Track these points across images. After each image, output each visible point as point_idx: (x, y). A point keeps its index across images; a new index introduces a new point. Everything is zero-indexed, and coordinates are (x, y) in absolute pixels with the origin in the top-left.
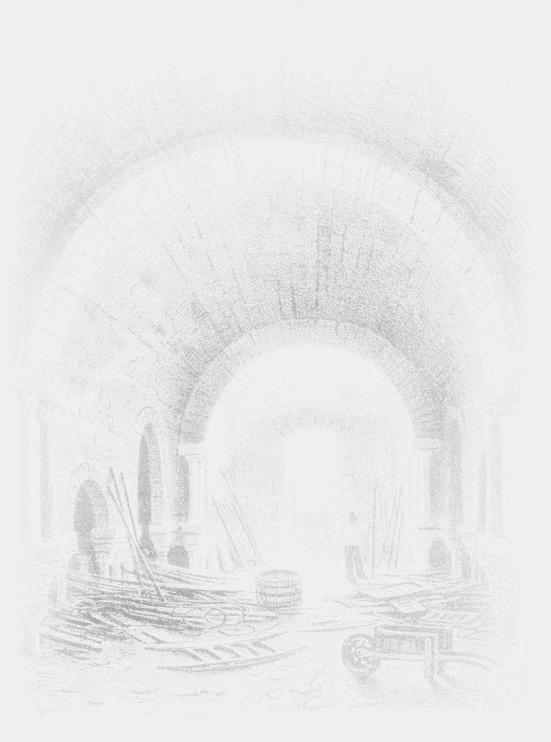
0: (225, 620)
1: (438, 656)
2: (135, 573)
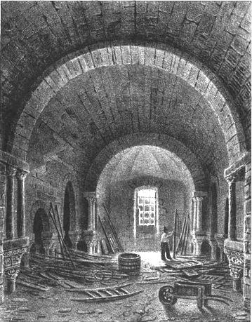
0: (104, 277)
1: (204, 297)
2: (62, 254)
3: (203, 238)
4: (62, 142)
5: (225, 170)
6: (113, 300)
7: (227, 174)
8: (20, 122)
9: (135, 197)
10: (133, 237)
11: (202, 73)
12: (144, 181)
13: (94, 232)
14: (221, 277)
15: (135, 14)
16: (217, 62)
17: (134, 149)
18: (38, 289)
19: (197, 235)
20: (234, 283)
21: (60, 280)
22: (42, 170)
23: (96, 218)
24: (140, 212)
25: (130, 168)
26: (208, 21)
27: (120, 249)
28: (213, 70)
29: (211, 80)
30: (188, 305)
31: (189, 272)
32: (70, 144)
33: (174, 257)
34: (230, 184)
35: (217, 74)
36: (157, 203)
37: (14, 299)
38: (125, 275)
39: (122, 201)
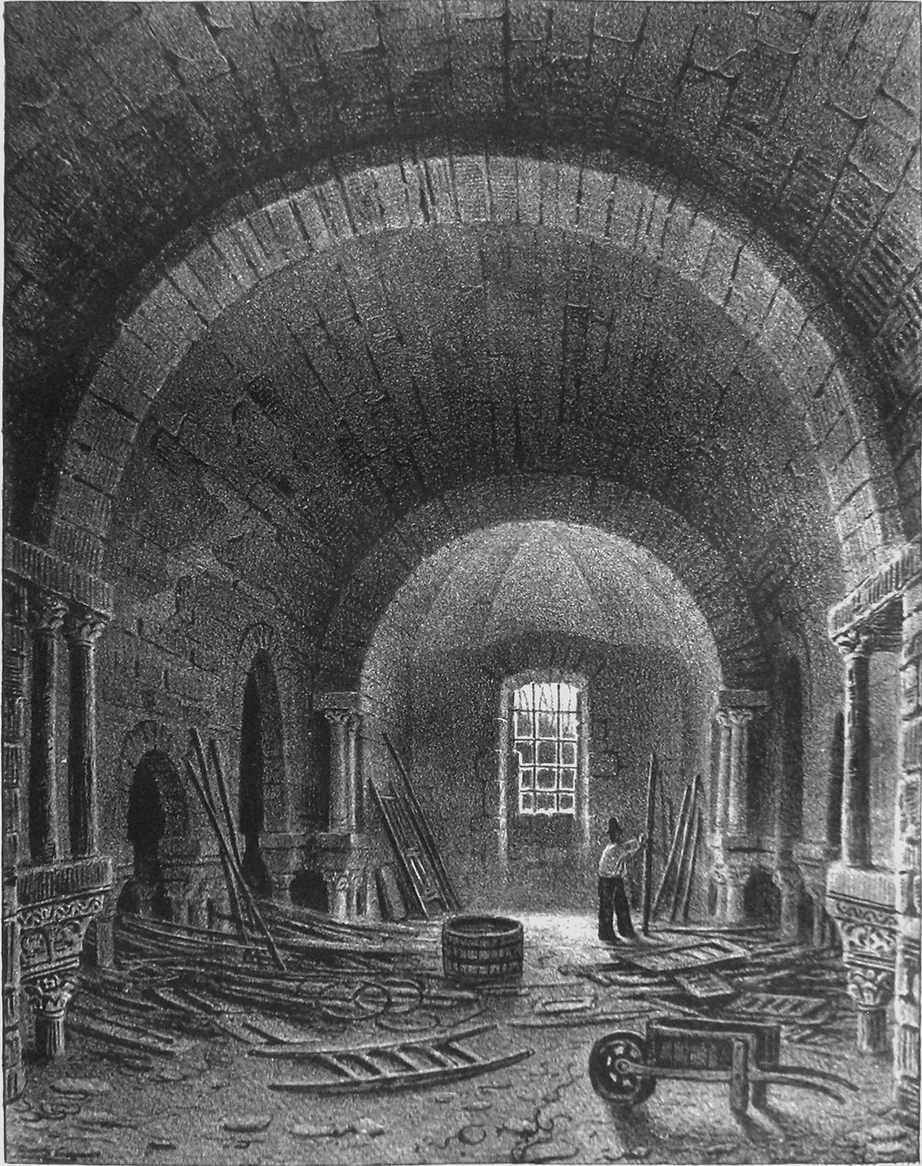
1: (754, 1072)
2: (233, 918)
3: (751, 859)
4: (237, 508)
5: (832, 611)
6: (417, 1084)
7: (838, 622)
8: (79, 431)
9: (504, 709)
10: (495, 858)
11: (747, 254)
12: (541, 649)
13: (353, 838)
14: (814, 1002)
15: (507, 44)
16: (802, 218)
17: (503, 532)
18: (147, 1048)
19: (731, 849)
20: (861, 1025)
21: (231, 1016)
22: (161, 609)
23: (359, 788)
24: (524, 766)
25: (484, 602)
26: (767, 67)
27: (448, 900)
28: (788, 242)
29: (783, 281)
30: (695, 1104)
31: (699, 983)
32: (267, 516)
33: (646, 932)
34: (849, 660)
35: (803, 258)
36: (586, 732)
37: (62, 1084)
38: (467, 994)
39: (454, 723)
